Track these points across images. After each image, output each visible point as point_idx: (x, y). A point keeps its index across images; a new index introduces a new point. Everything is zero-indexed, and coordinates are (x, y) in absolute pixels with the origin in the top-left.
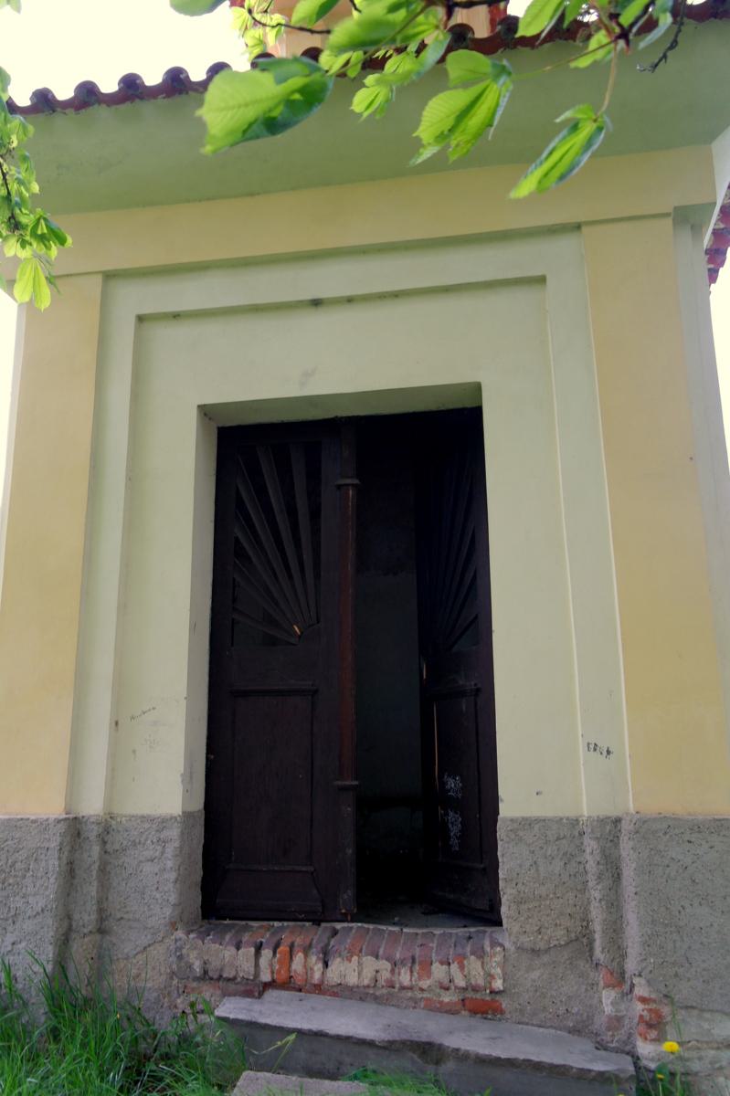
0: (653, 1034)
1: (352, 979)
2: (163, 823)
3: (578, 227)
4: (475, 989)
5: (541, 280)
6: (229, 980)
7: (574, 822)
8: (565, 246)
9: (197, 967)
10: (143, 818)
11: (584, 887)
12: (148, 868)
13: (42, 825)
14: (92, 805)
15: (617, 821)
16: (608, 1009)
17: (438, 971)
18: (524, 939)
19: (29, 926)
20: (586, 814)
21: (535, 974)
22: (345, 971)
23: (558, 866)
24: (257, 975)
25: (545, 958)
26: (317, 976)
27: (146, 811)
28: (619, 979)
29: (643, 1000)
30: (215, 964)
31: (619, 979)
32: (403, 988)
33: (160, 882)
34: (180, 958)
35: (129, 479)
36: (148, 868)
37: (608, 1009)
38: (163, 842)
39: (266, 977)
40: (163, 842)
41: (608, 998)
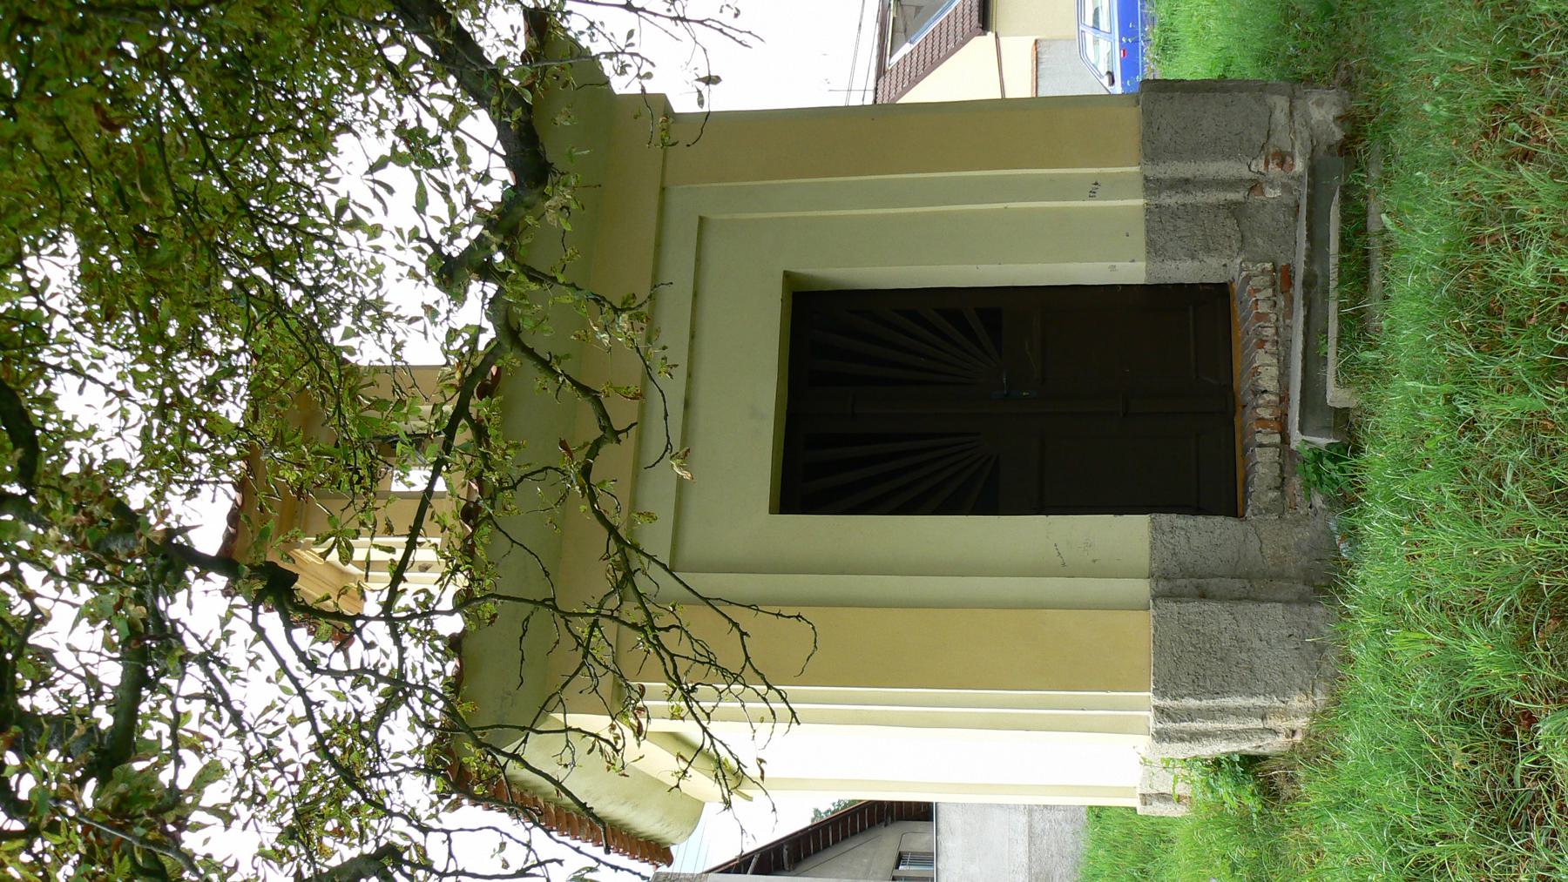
0: (1289, 159)
1: (1274, 371)
2: (1155, 528)
3: (663, 189)
4: (1274, 283)
5: (701, 219)
6: (1282, 470)
7: (1148, 211)
8: (676, 199)
9: (1273, 495)
10: (1153, 547)
11: (1196, 207)
12: (1195, 542)
13: (1160, 621)
14: (1142, 588)
15: (1146, 178)
16: (1278, 193)
17: (1263, 308)
18: (1236, 246)
19: (1245, 628)
20: (1140, 202)
21: (1260, 242)
22: (1268, 379)
23: (1180, 223)
24: (1275, 445)
25: (1248, 234)
26: (1273, 398)
27: (1147, 546)
28: (1255, 186)
29: (1267, 163)
30: (1269, 481)
31: (1255, 186)
32: (1277, 333)
33: (1202, 536)
34: (1267, 510)
35: (843, 573)
36: (1195, 542)
37: (1278, 193)
38: (1173, 529)
39: (1277, 438)
40: (1173, 529)
41: (1272, 193)
